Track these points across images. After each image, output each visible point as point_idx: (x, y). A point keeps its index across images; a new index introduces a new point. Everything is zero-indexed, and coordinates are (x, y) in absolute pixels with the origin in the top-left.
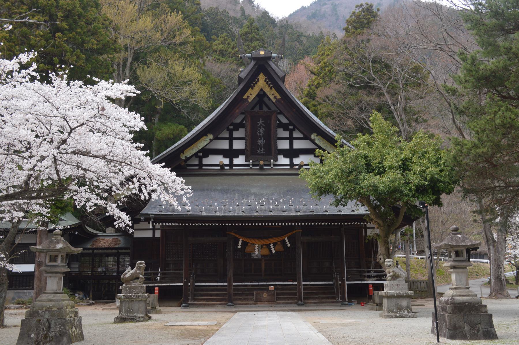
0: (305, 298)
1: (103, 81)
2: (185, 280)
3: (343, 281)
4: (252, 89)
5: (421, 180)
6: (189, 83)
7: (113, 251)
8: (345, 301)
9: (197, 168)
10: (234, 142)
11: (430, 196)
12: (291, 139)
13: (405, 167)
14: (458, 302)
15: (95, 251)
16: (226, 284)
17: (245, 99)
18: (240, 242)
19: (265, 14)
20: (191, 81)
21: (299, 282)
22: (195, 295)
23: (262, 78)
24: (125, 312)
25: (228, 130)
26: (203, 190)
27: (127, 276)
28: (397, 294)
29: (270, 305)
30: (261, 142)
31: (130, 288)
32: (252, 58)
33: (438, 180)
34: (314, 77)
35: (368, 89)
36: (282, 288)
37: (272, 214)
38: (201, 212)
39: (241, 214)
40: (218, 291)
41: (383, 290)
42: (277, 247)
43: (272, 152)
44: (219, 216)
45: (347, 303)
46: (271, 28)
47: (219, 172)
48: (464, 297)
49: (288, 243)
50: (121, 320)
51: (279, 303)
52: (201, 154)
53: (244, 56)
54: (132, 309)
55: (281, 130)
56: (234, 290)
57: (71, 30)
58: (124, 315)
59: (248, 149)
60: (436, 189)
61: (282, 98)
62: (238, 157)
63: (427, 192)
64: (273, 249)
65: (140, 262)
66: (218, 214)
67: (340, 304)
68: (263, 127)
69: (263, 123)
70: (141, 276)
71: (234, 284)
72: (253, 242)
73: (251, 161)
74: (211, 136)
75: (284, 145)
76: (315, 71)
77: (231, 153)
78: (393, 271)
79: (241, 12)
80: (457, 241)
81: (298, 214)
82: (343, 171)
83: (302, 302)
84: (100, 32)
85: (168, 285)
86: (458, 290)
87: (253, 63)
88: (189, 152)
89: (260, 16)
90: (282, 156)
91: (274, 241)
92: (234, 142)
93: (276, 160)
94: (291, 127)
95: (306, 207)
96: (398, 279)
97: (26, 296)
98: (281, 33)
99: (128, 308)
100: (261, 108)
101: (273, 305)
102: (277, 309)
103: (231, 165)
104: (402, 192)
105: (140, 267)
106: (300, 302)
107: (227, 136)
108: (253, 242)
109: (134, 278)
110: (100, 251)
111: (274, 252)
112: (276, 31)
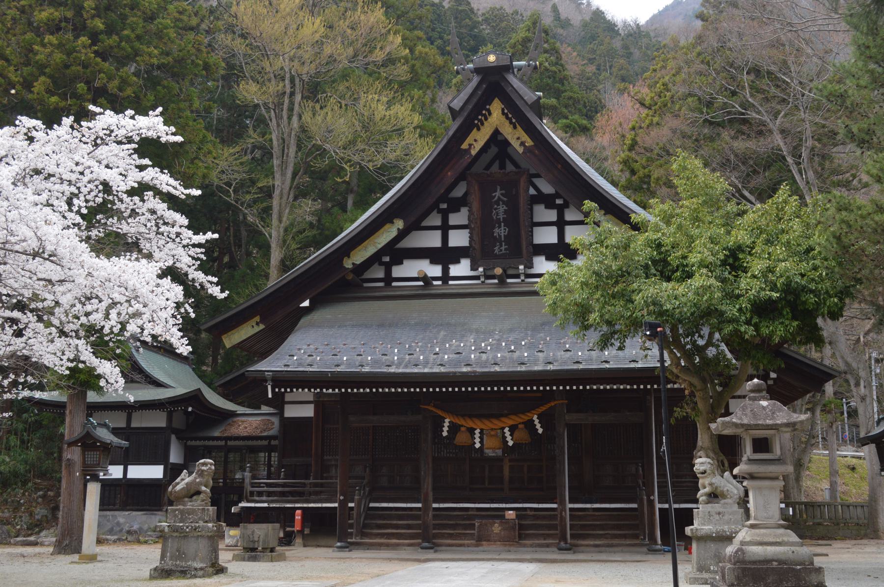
0: (572, 536)
1: (108, 112)
2: (342, 498)
3: (651, 503)
4: (479, 129)
5: (765, 290)
6: (399, 131)
7: (260, 443)
8: (656, 543)
9: (381, 284)
10: (452, 233)
11: (787, 322)
12: (561, 224)
13: (734, 261)
14: (753, 559)
15: (230, 443)
16: (420, 505)
17: (465, 150)
18: (446, 424)
19: (598, 15)
20: (403, 128)
21: (562, 503)
22: (365, 526)
23: (496, 107)
24: (171, 559)
25: (440, 211)
26: (381, 326)
27: (178, 488)
28: (717, 532)
29: (507, 548)
30: (501, 231)
31: (182, 512)
32: (477, 71)
33: (804, 287)
34: (644, 112)
35: (736, 126)
36: (534, 516)
37: (497, 369)
38: (362, 366)
39: (436, 370)
40: (413, 519)
41: (693, 524)
42: (517, 434)
43: (523, 250)
44: (394, 373)
45: (659, 547)
46: (607, 40)
47: (420, 292)
48: (769, 548)
49: (538, 426)
50: (162, 573)
51: (525, 546)
52: (387, 259)
53: (463, 69)
54: (184, 553)
55: (542, 207)
56: (435, 516)
57: (110, 30)
58: (169, 564)
59: (477, 246)
60: (801, 308)
61: (535, 145)
62: (459, 262)
63: (781, 315)
64: (509, 438)
65: (202, 461)
66: (392, 370)
67: (645, 549)
68: (504, 203)
69: (502, 194)
70: (203, 488)
71: (435, 505)
72: (470, 424)
73: (481, 269)
74: (399, 224)
75: (547, 236)
76: (648, 102)
77: (445, 256)
78: (711, 484)
79: (552, 14)
80: (755, 415)
81: (550, 367)
82: (597, 274)
83: (566, 543)
84: (167, 34)
85: (319, 505)
86: (757, 531)
87: (476, 80)
88: (360, 256)
89: (587, 18)
90: (543, 258)
91: (511, 423)
92: (452, 233)
93: (530, 265)
94: (559, 201)
95: (569, 354)
96: (723, 501)
97: (108, 521)
98: (626, 47)
99: (178, 550)
100: (502, 166)
101: (512, 548)
102: (464, 557)
103: (446, 277)
104: (722, 314)
105: (203, 471)
106: (563, 544)
107: (438, 223)
108: (470, 424)
109: (193, 493)
110: (237, 443)
111: (511, 443)
112: (617, 44)
